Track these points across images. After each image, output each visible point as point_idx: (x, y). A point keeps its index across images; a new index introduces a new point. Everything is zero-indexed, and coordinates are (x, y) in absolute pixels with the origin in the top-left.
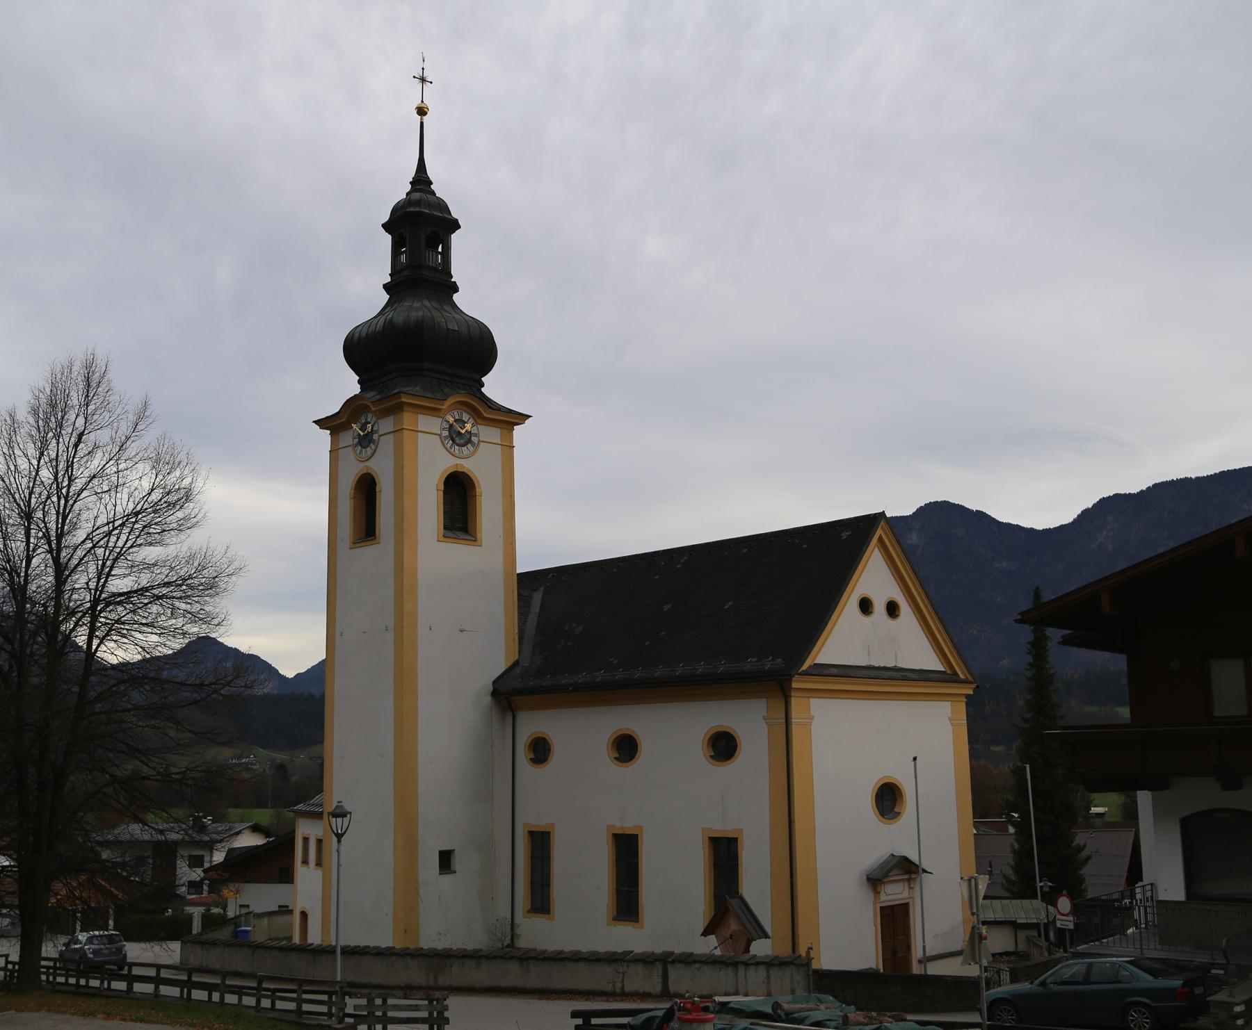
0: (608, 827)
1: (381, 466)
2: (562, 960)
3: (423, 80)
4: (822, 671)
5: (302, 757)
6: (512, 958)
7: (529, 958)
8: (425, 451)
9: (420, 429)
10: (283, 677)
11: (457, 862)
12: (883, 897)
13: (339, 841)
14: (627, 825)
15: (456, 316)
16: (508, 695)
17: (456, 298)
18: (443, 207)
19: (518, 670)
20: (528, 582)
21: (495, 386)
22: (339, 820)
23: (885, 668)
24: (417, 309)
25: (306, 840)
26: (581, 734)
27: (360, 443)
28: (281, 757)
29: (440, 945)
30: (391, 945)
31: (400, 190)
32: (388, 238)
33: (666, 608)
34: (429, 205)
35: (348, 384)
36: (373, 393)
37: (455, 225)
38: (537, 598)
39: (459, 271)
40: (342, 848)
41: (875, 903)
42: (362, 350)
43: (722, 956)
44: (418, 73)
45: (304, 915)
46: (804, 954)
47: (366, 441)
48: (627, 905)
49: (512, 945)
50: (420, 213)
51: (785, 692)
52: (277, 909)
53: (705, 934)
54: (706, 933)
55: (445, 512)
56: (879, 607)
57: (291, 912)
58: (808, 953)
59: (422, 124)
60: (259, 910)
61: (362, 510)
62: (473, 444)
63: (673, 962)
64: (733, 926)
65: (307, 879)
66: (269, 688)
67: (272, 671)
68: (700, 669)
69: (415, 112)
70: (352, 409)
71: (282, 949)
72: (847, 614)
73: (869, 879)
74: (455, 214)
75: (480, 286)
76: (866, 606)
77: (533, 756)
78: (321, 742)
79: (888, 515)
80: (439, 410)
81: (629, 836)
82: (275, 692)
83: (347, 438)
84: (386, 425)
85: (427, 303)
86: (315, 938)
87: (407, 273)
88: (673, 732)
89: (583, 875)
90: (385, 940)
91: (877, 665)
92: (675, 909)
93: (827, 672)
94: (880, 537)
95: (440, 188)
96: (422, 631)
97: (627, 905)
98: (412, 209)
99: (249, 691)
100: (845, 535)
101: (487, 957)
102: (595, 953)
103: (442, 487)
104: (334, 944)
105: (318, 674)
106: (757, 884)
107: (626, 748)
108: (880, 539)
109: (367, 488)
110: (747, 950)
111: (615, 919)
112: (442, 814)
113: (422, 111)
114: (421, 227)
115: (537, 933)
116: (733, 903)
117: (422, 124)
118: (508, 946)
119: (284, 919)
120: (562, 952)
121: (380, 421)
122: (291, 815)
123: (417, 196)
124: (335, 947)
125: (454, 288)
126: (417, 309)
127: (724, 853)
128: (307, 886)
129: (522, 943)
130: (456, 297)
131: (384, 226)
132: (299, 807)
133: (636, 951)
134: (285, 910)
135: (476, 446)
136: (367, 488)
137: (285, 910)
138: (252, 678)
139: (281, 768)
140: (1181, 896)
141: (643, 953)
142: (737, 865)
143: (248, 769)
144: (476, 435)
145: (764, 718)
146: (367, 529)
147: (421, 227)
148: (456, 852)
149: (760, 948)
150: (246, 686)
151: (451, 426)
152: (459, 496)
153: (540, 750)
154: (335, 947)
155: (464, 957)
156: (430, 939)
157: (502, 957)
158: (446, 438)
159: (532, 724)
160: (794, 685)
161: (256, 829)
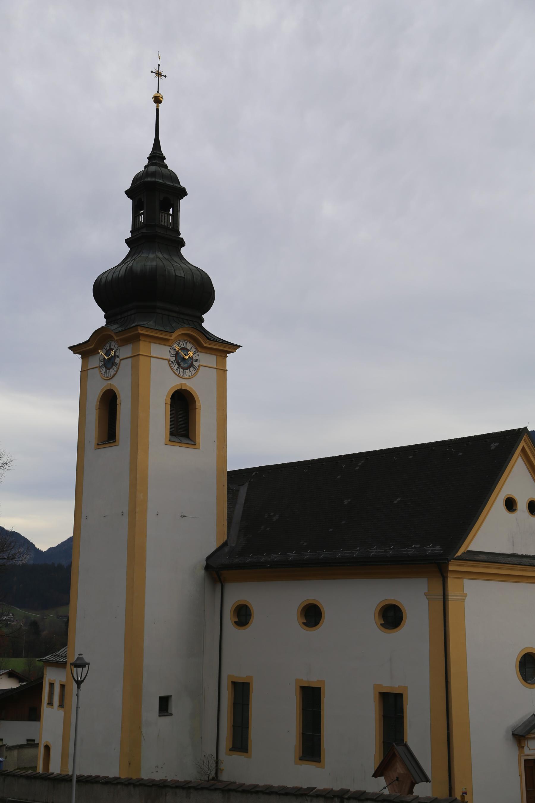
0: (297, 680)
1: (121, 384)
2: (276, 793)
3: (159, 74)
4: (474, 557)
5: (51, 616)
6: (216, 789)
7: (230, 790)
8: (157, 373)
9: (152, 355)
10: (38, 551)
11: (174, 706)
12: (527, 751)
13: (79, 687)
14: (312, 679)
15: (183, 265)
16: (219, 570)
17: (183, 251)
18: (173, 178)
19: (226, 550)
20: (237, 478)
21: (213, 322)
22: (80, 669)
23: (526, 557)
24: (152, 260)
25: (52, 685)
26: (276, 602)
27: (105, 365)
28: (34, 615)
29: (158, 777)
30: (117, 776)
31: (140, 164)
32: (129, 202)
33: (346, 502)
34: (162, 176)
35: (97, 318)
36: (115, 326)
37: (183, 193)
38: (243, 491)
39: (185, 230)
40: (81, 693)
41: (520, 756)
42: (106, 291)
43: (389, 796)
44: (155, 68)
45: (47, 748)
46: (459, 798)
47: (109, 363)
48: (311, 747)
49: (216, 778)
50: (155, 182)
51: (442, 573)
52: (25, 742)
53: (375, 775)
54: (376, 775)
55: (171, 421)
56: (522, 505)
57: (37, 745)
58: (463, 797)
59: (158, 110)
60: (10, 743)
61: (105, 419)
62: (195, 368)
63: (349, 798)
64: (399, 769)
65: (51, 717)
66: (27, 559)
67: (29, 545)
68: (373, 552)
69: (152, 100)
70: (99, 338)
71: (28, 777)
72: (495, 510)
73: (514, 735)
74: (183, 183)
75: (201, 245)
76: (510, 504)
77: (237, 620)
78: (67, 603)
79: (530, 429)
80: (168, 340)
81: (313, 688)
82: (32, 562)
83: (95, 361)
84: (125, 351)
85: (160, 255)
86: (55, 768)
87: (144, 230)
88: (350, 602)
89: (275, 720)
90: (112, 771)
91: (520, 554)
92: (352, 749)
93: (477, 558)
94: (523, 447)
95: (172, 162)
96: (151, 516)
97: (311, 747)
98: (149, 179)
99: (11, 562)
100: (494, 446)
101: (196, 788)
102: (284, 788)
103: (169, 402)
104: (70, 773)
105: (66, 548)
106: (418, 735)
107: (312, 615)
108: (523, 449)
109: (109, 402)
110: (411, 792)
111: (301, 759)
112: (162, 669)
113: (157, 100)
114: (156, 194)
115: (239, 769)
116: (400, 749)
117: (158, 110)
118: (213, 779)
119: (29, 752)
120: (257, 786)
121: (121, 348)
122: (41, 664)
123: (153, 169)
124: (72, 776)
125: (182, 243)
126: (152, 260)
127: (392, 706)
128: (51, 723)
129: (225, 777)
130: (183, 251)
131: (127, 192)
132: (47, 658)
133: (318, 788)
134: (32, 744)
135: (197, 370)
136: (109, 402)
137: (32, 744)
138: (13, 552)
139: (34, 625)
140: (229, 469)
141: (325, 790)
142: (403, 722)
143: (7, 625)
144: (197, 361)
145: (426, 595)
146: (109, 433)
147: (156, 194)
148: (173, 698)
149: (422, 790)
150: (8, 558)
151: (177, 353)
152: (182, 406)
153: (243, 616)
154: (72, 776)
155: (177, 787)
156: (148, 772)
157: (208, 789)
158: (173, 362)
159: (237, 593)
160: (451, 568)
161: (11, 675)
